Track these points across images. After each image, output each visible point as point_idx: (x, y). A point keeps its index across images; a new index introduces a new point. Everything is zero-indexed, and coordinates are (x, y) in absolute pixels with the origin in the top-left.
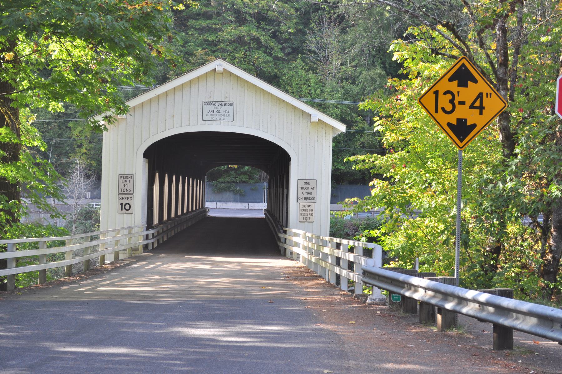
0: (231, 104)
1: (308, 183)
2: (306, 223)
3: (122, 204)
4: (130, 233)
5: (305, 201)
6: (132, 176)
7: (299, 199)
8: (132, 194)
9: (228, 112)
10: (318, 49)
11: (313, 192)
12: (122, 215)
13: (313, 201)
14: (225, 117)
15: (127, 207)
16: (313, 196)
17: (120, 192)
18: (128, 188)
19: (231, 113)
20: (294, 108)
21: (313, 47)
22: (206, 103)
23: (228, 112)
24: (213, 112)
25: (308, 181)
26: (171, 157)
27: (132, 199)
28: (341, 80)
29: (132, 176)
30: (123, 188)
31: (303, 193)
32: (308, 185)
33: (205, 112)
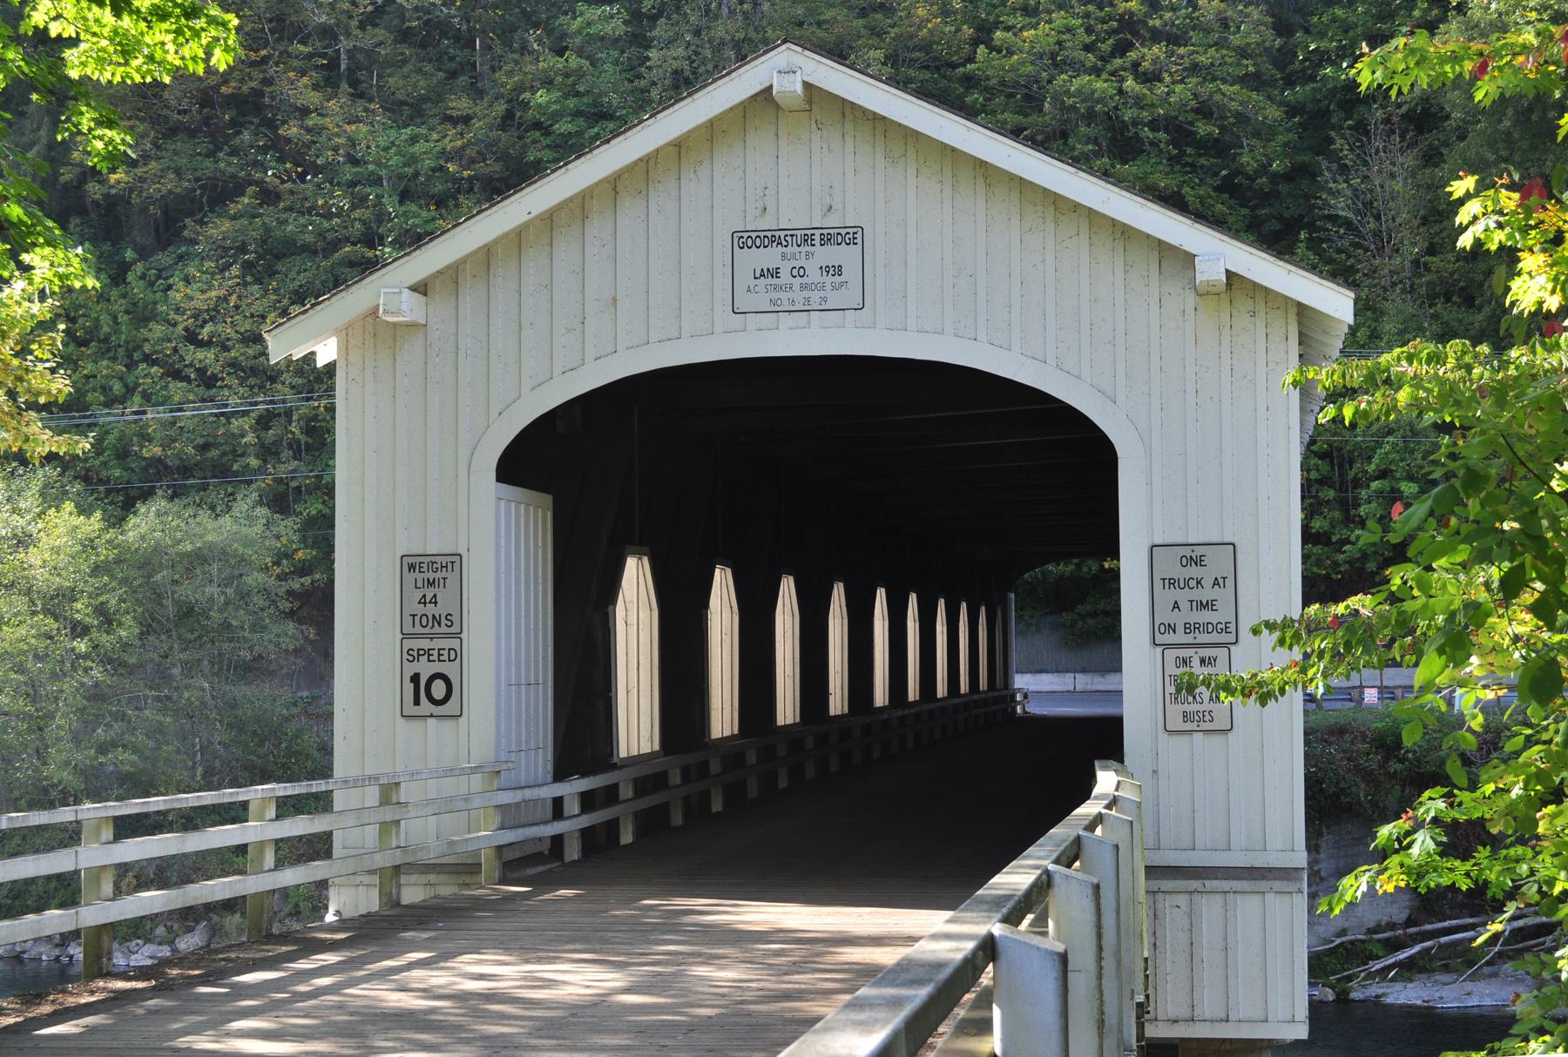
0: (849, 236)
1: (1198, 561)
2: (1198, 737)
3: (415, 679)
4: (385, 801)
5: (1189, 639)
6: (453, 562)
7: (1159, 629)
8: (457, 636)
9: (838, 270)
10: (1358, 212)
11: (1223, 596)
12: (417, 725)
13: (1223, 638)
14: (828, 293)
15: (439, 689)
16: (1223, 615)
17: (408, 629)
18: (439, 610)
19: (851, 273)
20: (1124, 232)
21: (1341, 207)
22: (746, 240)
23: (838, 270)
24: (775, 273)
25: (1199, 551)
26: (643, 472)
27: (455, 655)
28: (1431, 299)
29: (453, 562)
30: (420, 610)
31: (1176, 606)
32: (1196, 567)
33: (744, 278)
